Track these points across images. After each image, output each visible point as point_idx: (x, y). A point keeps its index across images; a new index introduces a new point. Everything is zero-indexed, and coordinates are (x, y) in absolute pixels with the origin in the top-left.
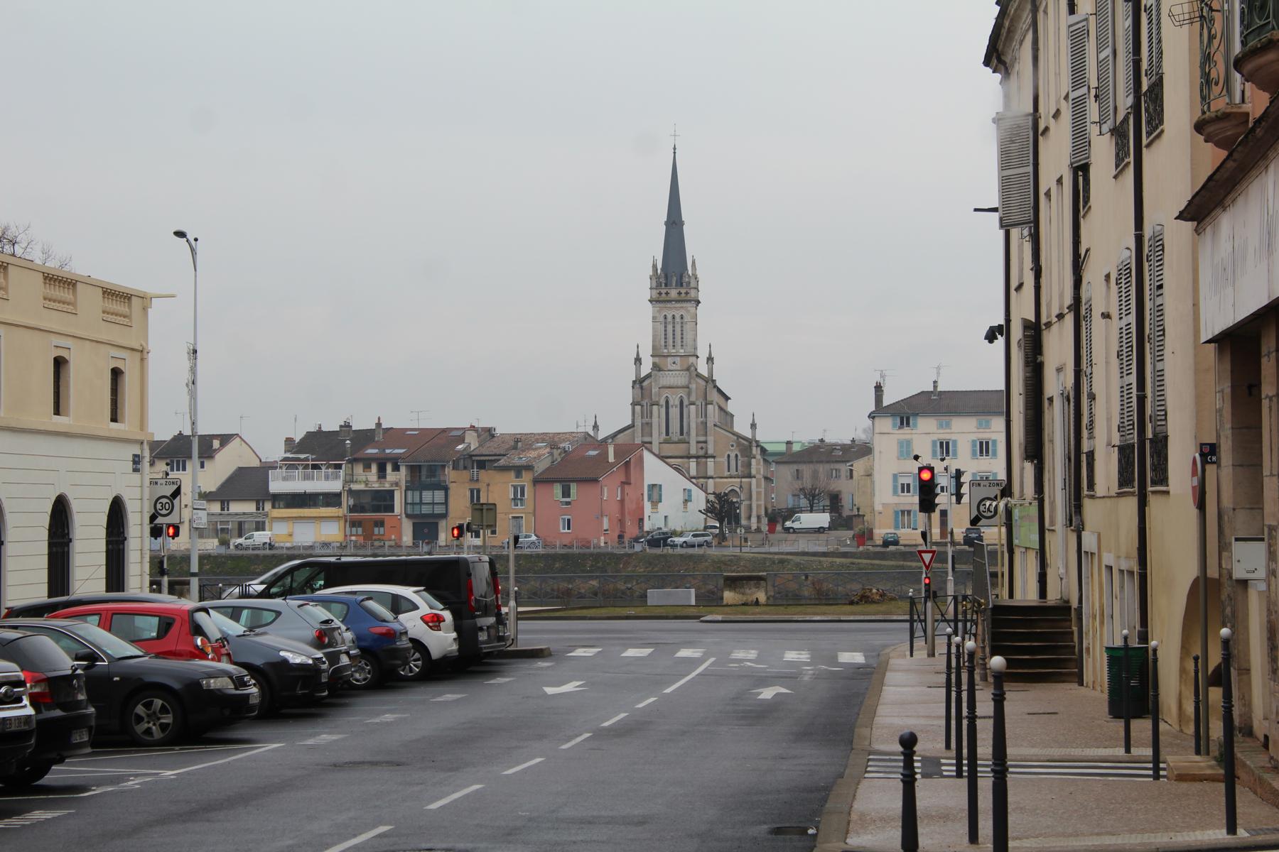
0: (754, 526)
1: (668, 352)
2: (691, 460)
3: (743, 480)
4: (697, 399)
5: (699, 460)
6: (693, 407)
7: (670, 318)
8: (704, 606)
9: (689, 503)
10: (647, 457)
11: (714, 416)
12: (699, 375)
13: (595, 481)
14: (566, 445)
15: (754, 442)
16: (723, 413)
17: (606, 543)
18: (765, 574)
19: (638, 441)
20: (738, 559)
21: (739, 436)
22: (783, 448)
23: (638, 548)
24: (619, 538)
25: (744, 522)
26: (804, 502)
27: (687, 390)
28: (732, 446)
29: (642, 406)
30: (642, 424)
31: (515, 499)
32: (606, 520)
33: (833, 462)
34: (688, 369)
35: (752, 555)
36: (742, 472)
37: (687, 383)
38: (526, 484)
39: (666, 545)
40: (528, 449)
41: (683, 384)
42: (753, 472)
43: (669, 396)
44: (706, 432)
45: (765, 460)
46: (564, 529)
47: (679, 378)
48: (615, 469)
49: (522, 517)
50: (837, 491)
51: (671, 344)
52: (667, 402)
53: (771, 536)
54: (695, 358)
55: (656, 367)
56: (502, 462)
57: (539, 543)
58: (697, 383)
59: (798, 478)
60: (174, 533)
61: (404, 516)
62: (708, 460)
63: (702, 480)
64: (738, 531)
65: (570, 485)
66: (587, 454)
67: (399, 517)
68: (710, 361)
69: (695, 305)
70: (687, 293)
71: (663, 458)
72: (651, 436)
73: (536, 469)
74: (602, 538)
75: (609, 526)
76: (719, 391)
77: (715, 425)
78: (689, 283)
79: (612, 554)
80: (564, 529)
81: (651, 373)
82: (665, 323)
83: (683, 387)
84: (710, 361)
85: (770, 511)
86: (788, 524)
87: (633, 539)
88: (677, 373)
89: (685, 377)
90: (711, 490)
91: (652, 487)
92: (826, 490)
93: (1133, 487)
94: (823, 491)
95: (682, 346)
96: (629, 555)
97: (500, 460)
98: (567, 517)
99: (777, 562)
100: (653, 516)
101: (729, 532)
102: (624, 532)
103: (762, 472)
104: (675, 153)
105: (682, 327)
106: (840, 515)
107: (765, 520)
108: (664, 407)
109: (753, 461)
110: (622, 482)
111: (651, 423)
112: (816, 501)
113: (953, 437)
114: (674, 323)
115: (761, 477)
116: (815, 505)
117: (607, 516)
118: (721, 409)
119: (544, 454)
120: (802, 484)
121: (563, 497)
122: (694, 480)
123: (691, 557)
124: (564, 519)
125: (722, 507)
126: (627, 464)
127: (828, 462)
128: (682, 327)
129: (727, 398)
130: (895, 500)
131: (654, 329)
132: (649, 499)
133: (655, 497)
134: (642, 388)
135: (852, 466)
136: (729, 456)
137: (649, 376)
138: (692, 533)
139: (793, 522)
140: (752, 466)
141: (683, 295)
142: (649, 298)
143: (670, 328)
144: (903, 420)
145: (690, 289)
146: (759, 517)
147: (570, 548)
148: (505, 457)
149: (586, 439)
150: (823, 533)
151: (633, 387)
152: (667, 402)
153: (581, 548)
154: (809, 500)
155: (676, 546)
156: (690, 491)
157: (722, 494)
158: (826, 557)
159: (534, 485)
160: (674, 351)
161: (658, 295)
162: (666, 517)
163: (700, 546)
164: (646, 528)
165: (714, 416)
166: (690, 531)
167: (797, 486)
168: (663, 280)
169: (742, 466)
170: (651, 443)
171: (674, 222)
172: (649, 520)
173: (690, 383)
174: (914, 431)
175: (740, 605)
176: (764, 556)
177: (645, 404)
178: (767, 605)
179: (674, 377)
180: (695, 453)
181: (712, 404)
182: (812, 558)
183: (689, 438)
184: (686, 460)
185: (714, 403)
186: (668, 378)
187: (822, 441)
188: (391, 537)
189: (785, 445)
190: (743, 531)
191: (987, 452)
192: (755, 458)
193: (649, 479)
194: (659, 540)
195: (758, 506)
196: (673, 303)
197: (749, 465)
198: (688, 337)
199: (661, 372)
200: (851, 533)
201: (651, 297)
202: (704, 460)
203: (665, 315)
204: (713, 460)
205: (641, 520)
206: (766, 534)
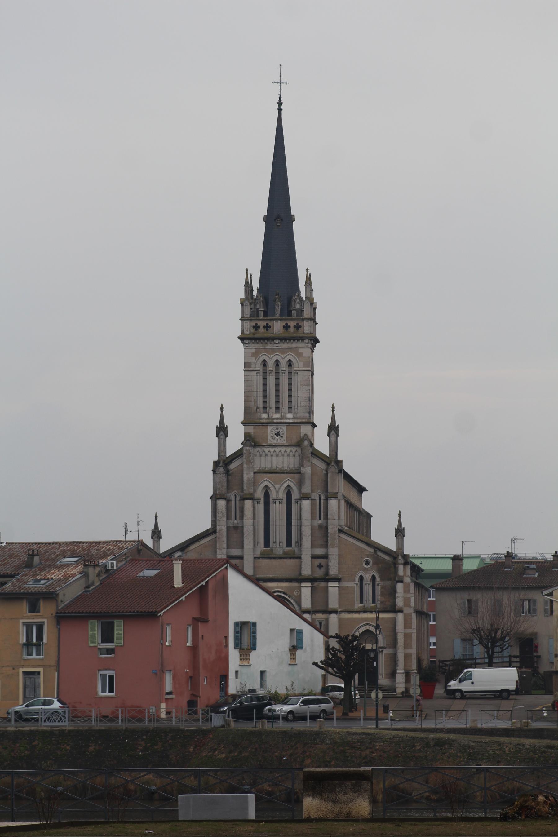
0: (400, 688)
1: (268, 418)
2: (303, 584)
3: (381, 616)
4: (312, 491)
5: (316, 584)
6: (306, 504)
7: (271, 365)
8: (266, 822)
9: (299, 652)
10: (234, 578)
11: (339, 518)
12: (316, 454)
13: (152, 616)
14: (109, 562)
15: (400, 557)
16: (353, 513)
17: (168, 713)
18: (369, 769)
19: (221, 554)
20: (373, 738)
21: (377, 548)
22: (447, 566)
23: (217, 721)
24: (189, 706)
25: (383, 681)
26: (479, 651)
27: (297, 476)
28: (367, 563)
29: (228, 501)
30: (228, 528)
31: (28, 644)
32: (168, 679)
33: (524, 588)
34: (299, 444)
35: (394, 733)
36: (382, 603)
37: (297, 465)
38: (45, 621)
39: (261, 716)
40: (50, 567)
41: (291, 466)
42: (400, 603)
43: (270, 485)
44: (327, 542)
45: (418, 586)
46: (104, 691)
47: (286, 458)
48: (183, 598)
49: (39, 673)
50: (532, 634)
51: (273, 404)
52: (267, 495)
53: (426, 703)
54: (309, 427)
55: (249, 440)
57: (64, 712)
58: (313, 466)
59: (470, 613)
62: (330, 584)
63: (320, 616)
64: (373, 695)
65: (113, 623)
66: (141, 574)
68: (333, 432)
69: (310, 346)
70: (298, 327)
71: (257, 581)
72: (242, 547)
73: (61, 597)
74: (163, 705)
75: (174, 687)
76: (348, 478)
77: (340, 531)
78: (301, 311)
79: (178, 731)
80: (104, 691)
81: (241, 450)
82: (265, 373)
83: (291, 472)
84: (333, 432)
85: (425, 663)
86: (453, 684)
87: (211, 707)
88: (283, 449)
89: (294, 456)
90: (333, 630)
91: (241, 626)
92: (512, 632)
93: (548, 614)
94: (508, 634)
95: (290, 408)
96: (204, 733)
97: (6, 583)
98: (108, 673)
99: (432, 743)
100: (243, 671)
101: (361, 697)
102: (197, 696)
103: (413, 604)
104: (280, 110)
105: (290, 379)
106: (535, 671)
107: (416, 679)
109: (400, 587)
110: (194, 618)
111: (243, 527)
112: (497, 649)
114: (277, 373)
115: (412, 611)
116: (495, 655)
117: (170, 670)
118: (350, 505)
119: (74, 575)
120: (476, 622)
121: (103, 642)
122: (307, 616)
123: (300, 734)
124: (104, 676)
125: (349, 657)
126: (203, 590)
127: (516, 588)
128: (290, 379)
129: (361, 489)
131: (247, 382)
132: (236, 646)
133: (246, 640)
134: (227, 473)
135: (551, 594)
136: (361, 578)
137: (238, 454)
138: (302, 699)
139: (461, 681)
140: (397, 595)
141: (292, 330)
142: (240, 334)
143: (271, 380)
145: (303, 320)
146: (407, 674)
147: (111, 720)
148: (14, 580)
149: (139, 551)
150: (507, 698)
151: (214, 472)
152: (267, 495)
153: (129, 721)
154: (486, 647)
155: (277, 718)
156: (300, 632)
157: (350, 638)
158: (508, 736)
159: (58, 623)
160: (278, 416)
161: (253, 330)
162: (262, 673)
163: (314, 717)
164: (232, 689)
165: (339, 518)
166: (301, 695)
167: (467, 626)
168: (261, 307)
169: (382, 594)
170: (241, 558)
171: (278, 217)
172: (237, 677)
173: (302, 465)
175: (332, 820)
176: (412, 734)
177: (233, 498)
178: (372, 820)
179: (277, 456)
180: (310, 573)
181: (336, 498)
182: (488, 739)
183: (300, 550)
184: (296, 585)
185: (340, 496)
186: (269, 458)
187: (509, 555)
189: (450, 561)
190: (380, 695)
192: (401, 581)
194: (250, 708)
195: (407, 657)
196: (277, 341)
197: (393, 592)
198: (300, 393)
199: (258, 449)
200: (549, 699)
201: (242, 333)
202: (323, 584)
203: (264, 361)
204: (336, 584)
205: (224, 678)
206: (417, 700)
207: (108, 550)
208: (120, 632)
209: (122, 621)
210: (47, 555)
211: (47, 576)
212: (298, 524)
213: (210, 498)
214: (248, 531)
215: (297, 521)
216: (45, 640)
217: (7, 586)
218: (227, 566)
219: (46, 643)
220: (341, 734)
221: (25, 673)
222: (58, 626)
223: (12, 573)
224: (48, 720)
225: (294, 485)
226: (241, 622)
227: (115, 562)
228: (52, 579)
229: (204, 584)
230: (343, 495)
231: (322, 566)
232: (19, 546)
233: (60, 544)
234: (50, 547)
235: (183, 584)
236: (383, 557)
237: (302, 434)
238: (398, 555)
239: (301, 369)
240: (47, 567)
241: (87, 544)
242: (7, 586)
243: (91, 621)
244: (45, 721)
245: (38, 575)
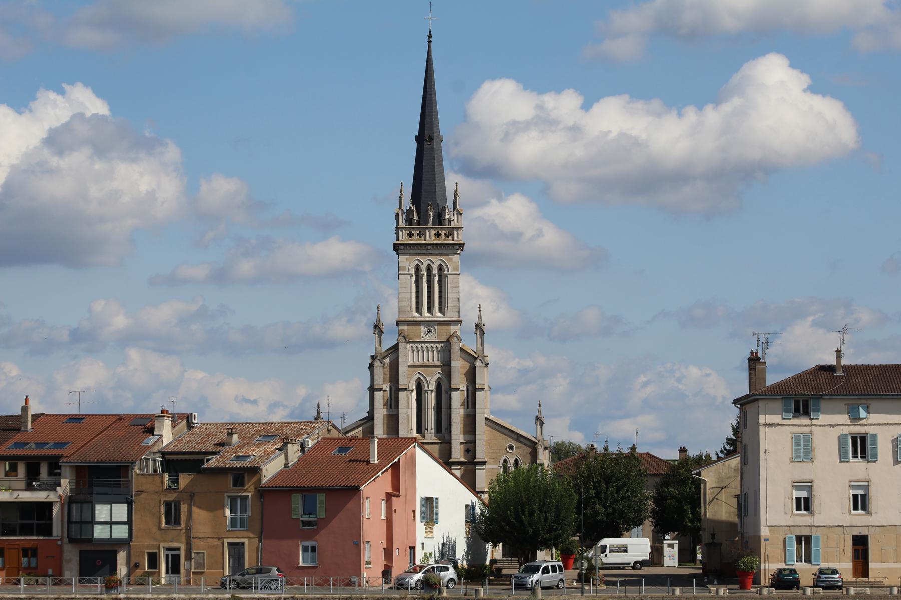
48: (380, 474)
61: (66, 540)
67: (59, 543)
104: (430, 42)
108: (415, 393)
113: (871, 431)
126: (396, 467)
130: (789, 521)
136: (505, 461)
174: (814, 422)
188: (47, 572)
191: (864, 452)
193: (423, 490)
208: (322, 506)
216: (249, 513)
217: (212, 462)
218: (415, 446)
219: (250, 515)
224: (264, 588)
226: (426, 498)
227: (310, 441)
228: (254, 456)
230: (489, 387)
233: (252, 424)
234: (244, 428)
237: (451, 331)
239: (450, 273)
240: (246, 445)
242: (212, 462)
244: (261, 589)
245: (239, 452)
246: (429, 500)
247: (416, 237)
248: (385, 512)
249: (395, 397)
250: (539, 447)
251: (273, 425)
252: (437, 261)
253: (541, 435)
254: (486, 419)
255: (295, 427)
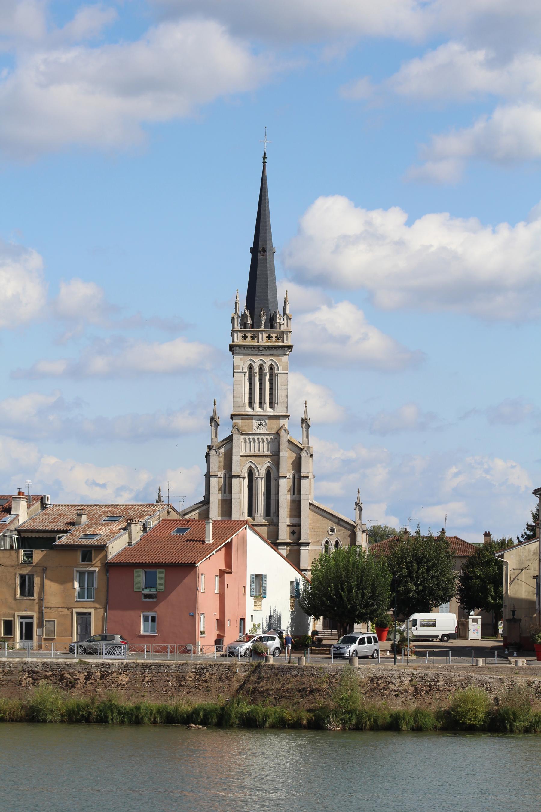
56: (64, 540)
60: (514, 718)
104: (264, 163)
136: (327, 542)
144: (29, 590)
148: (68, 535)
193: (252, 569)
207: (143, 511)
208: (162, 580)
209: (164, 570)
210: (91, 515)
211: (96, 532)
212: (276, 498)
213: (204, 476)
214: (235, 503)
215: (275, 495)
217: (63, 539)
218: (246, 527)
220: (373, 670)
221: (78, 614)
222: (108, 574)
223: (65, 529)
224: (109, 654)
225: (273, 466)
228: (101, 534)
229: (230, 541)
231: (295, 533)
232: (65, 507)
233: (100, 506)
234: (92, 509)
235: (212, 540)
236: (345, 526)
238: (357, 525)
241: (124, 507)
242: (63, 539)
243: (136, 570)
244: (106, 654)
246: (258, 576)
247: (249, 339)
248: (218, 587)
249: (228, 483)
250: (358, 530)
251: (118, 507)
252: (268, 361)
253: (360, 519)
254: (310, 504)
255: (138, 509)
